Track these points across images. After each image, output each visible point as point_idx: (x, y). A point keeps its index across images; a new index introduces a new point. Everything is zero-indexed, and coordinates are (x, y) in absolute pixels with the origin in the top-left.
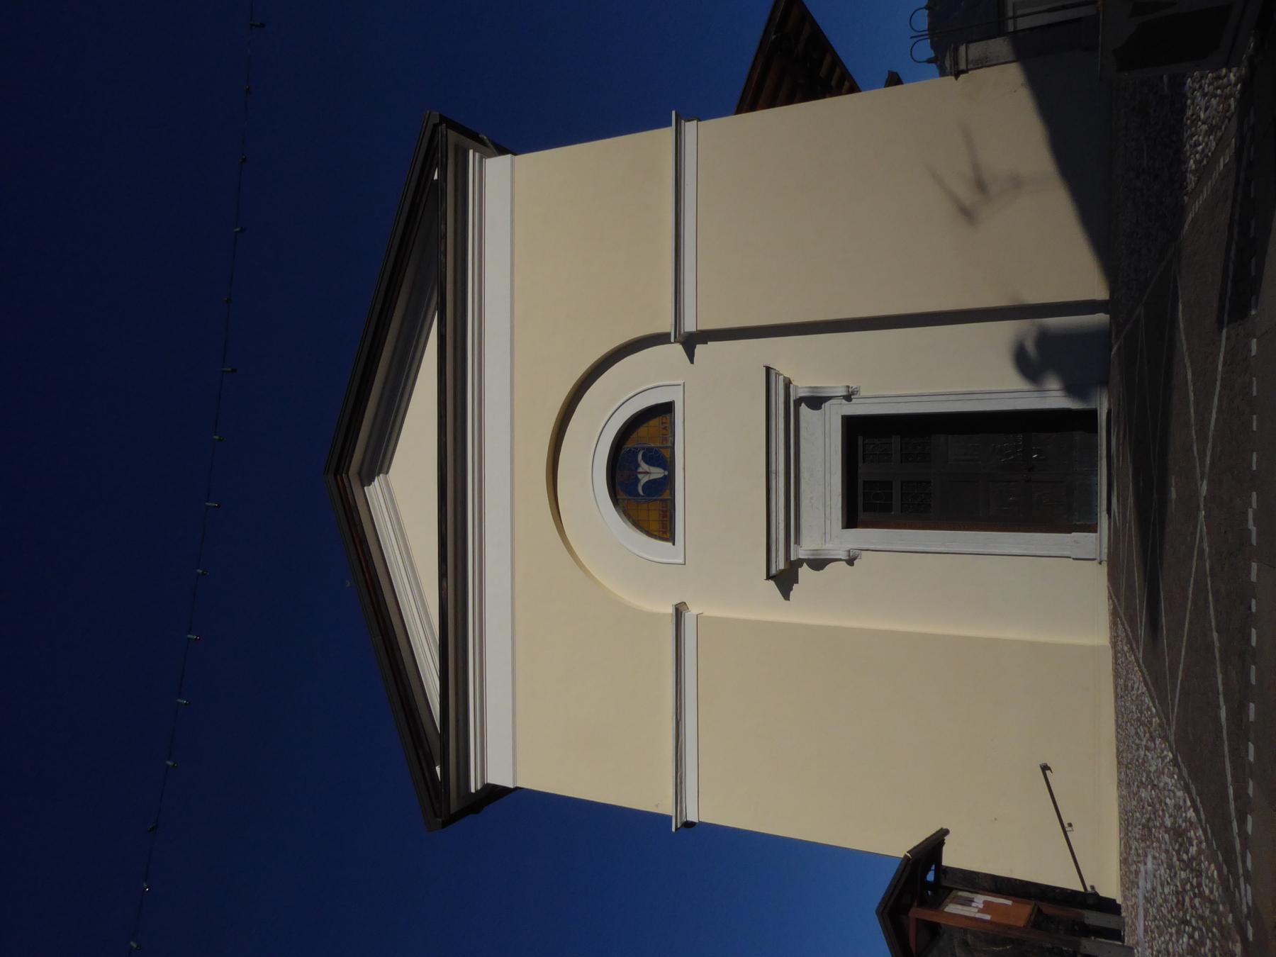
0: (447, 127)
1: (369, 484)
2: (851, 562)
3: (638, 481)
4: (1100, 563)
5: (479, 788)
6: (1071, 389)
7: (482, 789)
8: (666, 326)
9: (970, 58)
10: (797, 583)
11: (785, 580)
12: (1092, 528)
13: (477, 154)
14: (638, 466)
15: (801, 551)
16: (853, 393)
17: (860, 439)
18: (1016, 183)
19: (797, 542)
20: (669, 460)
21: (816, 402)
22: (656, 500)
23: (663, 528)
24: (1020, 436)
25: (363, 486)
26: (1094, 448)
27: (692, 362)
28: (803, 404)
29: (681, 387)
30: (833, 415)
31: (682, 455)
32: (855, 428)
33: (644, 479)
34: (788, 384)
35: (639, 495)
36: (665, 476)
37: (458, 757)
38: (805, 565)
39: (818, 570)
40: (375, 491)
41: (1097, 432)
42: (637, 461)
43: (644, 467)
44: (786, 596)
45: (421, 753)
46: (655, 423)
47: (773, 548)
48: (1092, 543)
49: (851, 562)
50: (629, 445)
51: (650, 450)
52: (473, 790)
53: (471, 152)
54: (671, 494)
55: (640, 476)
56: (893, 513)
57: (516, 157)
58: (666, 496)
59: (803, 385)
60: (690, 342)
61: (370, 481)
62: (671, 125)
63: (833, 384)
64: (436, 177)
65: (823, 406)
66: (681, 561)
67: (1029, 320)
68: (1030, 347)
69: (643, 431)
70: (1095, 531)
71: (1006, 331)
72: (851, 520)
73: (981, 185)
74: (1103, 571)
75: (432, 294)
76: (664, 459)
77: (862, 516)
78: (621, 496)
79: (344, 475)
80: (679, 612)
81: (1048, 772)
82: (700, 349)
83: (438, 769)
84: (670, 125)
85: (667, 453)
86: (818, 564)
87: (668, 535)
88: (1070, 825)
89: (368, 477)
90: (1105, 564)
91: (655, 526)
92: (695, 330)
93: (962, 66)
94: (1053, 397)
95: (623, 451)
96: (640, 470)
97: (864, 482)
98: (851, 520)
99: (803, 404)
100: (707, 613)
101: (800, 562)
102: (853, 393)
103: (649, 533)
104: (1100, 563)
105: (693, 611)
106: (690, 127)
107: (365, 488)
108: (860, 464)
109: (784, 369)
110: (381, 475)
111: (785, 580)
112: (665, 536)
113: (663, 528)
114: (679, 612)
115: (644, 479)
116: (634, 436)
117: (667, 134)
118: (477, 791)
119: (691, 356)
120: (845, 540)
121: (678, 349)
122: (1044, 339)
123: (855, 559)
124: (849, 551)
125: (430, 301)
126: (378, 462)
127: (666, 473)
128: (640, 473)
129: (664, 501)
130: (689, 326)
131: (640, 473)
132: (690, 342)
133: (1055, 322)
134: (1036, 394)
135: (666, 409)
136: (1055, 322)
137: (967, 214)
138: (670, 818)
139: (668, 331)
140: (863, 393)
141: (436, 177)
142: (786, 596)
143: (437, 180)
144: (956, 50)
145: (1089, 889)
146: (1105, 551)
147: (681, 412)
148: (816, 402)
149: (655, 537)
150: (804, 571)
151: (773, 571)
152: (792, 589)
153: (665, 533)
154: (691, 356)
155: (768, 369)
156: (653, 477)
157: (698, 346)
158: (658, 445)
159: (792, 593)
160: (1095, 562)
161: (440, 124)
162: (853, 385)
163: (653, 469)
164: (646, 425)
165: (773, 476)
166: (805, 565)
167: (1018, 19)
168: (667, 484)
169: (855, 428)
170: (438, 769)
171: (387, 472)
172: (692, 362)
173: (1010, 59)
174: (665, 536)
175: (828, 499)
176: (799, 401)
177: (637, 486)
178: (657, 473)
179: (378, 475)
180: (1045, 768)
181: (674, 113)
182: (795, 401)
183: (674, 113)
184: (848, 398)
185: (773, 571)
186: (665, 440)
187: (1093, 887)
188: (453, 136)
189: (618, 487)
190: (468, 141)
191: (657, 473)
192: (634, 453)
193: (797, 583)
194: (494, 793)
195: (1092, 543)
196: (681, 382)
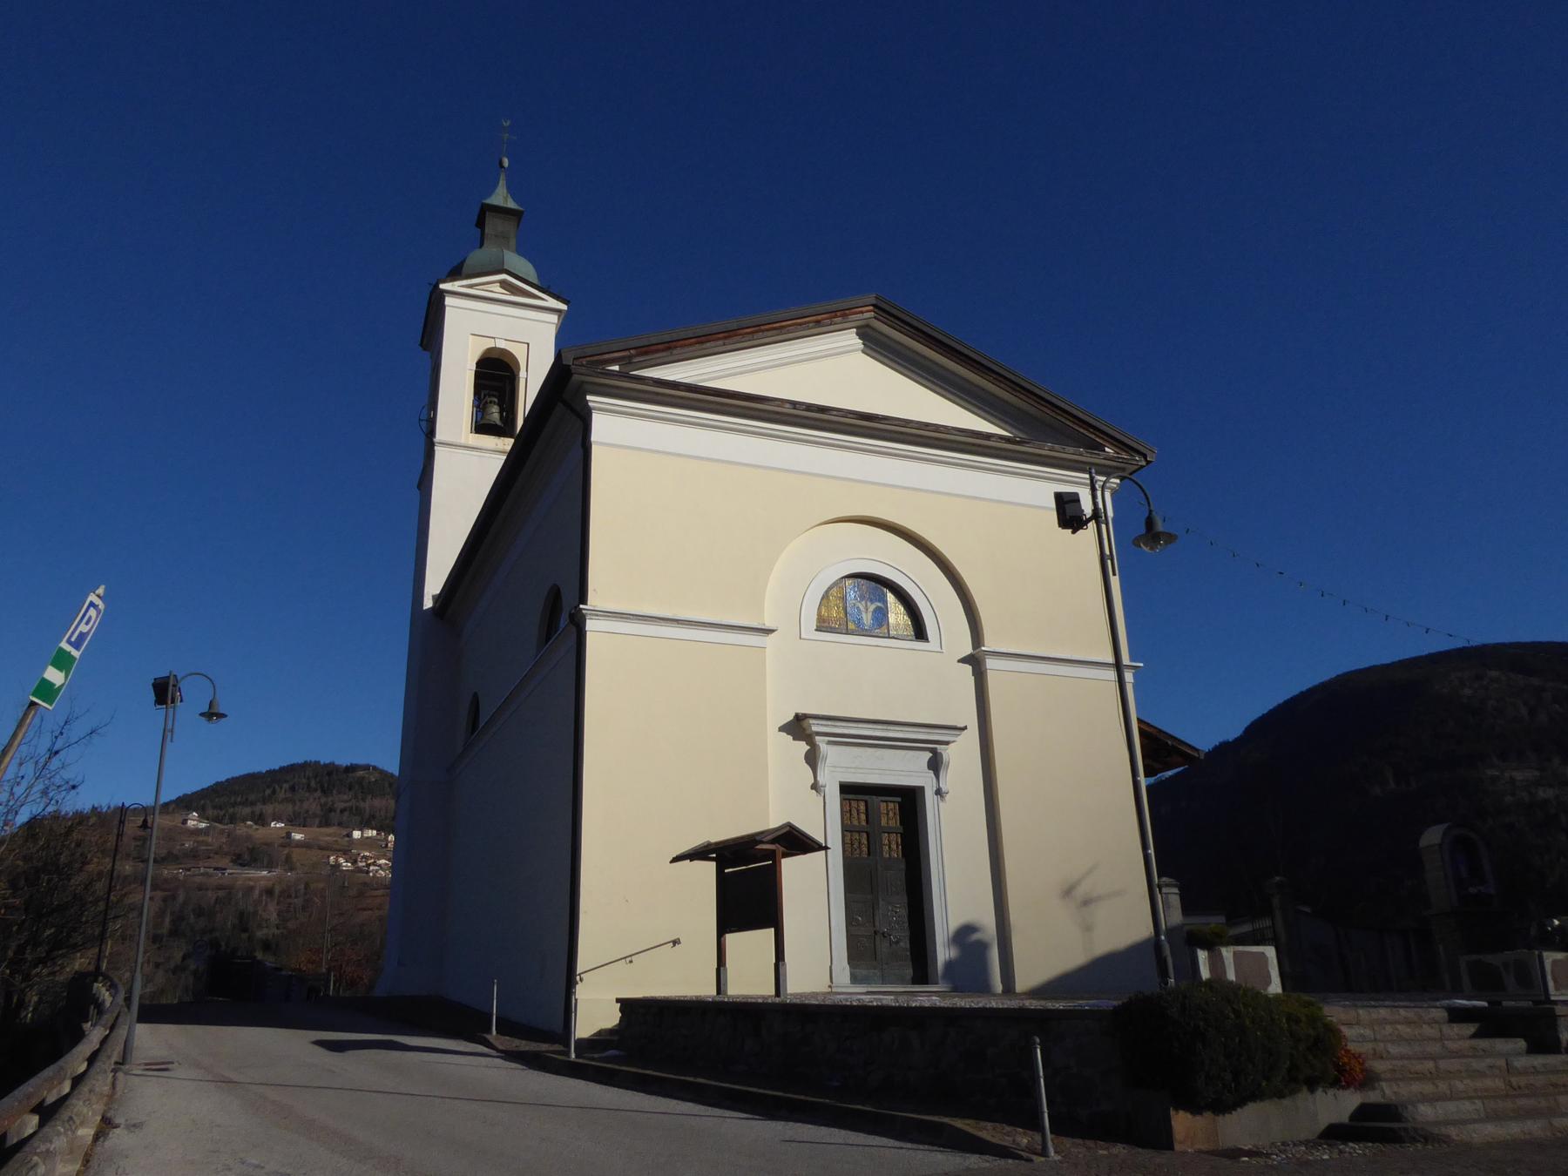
1: (857, 334)
2: (815, 787)
4: (830, 987)
6: (949, 965)
10: (794, 739)
11: (798, 727)
12: (855, 979)
16: (942, 797)
18: (1088, 928)
19: (829, 743)
21: (935, 764)
25: (857, 328)
28: (931, 755)
29: (939, 650)
31: (837, 640)
32: (909, 801)
34: (947, 743)
37: (617, 387)
39: (806, 762)
40: (850, 339)
44: (783, 729)
47: (829, 723)
49: (815, 787)
52: (588, 398)
57: (1220, 1118)
59: (949, 753)
61: (861, 335)
63: (949, 780)
65: (931, 771)
66: (803, 636)
67: (995, 933)
68: (975, 937)
71: (988, 920)
72: (847, 789)
73: (1086, 902)
75: (1010, 432)
80: (769, 631)
83: (616, 368)
86: (812, 759)
88: (631, 962)
89: (865, 334)
92: (988, 667)
93: (1164, 890)
94: (943, 952)
99: (931, 755)
102: (942, 797)
107: (855, 330)
110: (862, 346)
111: (798, 727)
114: (769, 631)
119: (963, 660)
121: (968, 650)
122: (983, 947)
125: (1006, 430)
126: (875, 345)
128: (866, 603)
130: (990, 663)
133: (994, 955)
134: (946, 940)
136: (994, 955)
137: (1068, 892)
138: (586, 604)
144: (1175, 886)
147: (920, 648)
148: (935, 764)
150: (803, 747)
152: (788, 734)
154: (963, 660)
159: (785, 734)
160: (830, 983)
162: (948, 797)
163: (870, 615)
165: (885, 727)
169: (909, 801)
170: (616, 368)
171: (863, 352)
175: (861, 771)
179: (863, 344)
180: (675, 942)
181: (1142, 665)
182: (936, 748)
183: (1142, 665)
184: (939, 792)
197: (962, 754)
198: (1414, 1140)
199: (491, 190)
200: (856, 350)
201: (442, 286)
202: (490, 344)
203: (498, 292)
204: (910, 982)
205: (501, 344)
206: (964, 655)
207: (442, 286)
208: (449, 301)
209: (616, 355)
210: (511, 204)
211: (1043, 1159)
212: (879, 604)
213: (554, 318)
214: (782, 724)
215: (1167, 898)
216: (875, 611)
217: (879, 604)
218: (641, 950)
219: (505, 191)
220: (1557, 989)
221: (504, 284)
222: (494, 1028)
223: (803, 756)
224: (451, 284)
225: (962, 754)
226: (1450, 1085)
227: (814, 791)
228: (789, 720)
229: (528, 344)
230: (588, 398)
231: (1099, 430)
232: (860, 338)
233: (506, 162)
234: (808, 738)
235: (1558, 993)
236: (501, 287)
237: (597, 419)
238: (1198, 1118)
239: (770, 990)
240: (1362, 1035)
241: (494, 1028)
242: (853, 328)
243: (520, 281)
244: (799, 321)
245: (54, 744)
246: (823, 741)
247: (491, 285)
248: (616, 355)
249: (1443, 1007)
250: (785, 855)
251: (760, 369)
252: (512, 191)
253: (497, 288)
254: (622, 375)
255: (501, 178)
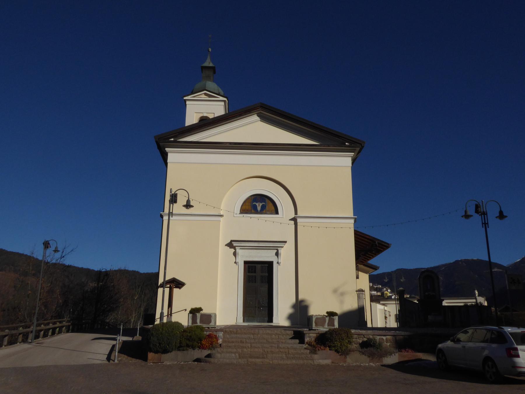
0: (360, 148)
1: (257, 116)
2: (235, 263)
3: (257, 202)
4: (236, 323)
5: (167, 151)
7: (166, 152)
8: (300, 214)
9: (360, 295)
10: (230, 248)
11: (230, 245)
12: (244, 321)
13: (353, 155)
14: (261, 203)
15: (238, 250)
17: (267, 265)
19: (240, 249)
20: (262, 212)
21: (277, 254)
22: (251, 208)
23: (244, 210)
24: (267, 305)
26: (264, 322)
27: (289, 220)
28: (277, 251)
29: (282, 217)
30: (273, 259)
32: (269, 266)
33: (257, 204)
34: (282, 247)
35: (253, 203)
36: (258, 211)
38: (234, 250)
41: (268, 322)
42: (263, 202)
43: (261, 204)
44: (226, 245)
45: (177, 134)
46: (273, 208)
48: (240, 321)
49: (235, 263)
50: (267, 200)
51: (265, 207)
52: (166, 149)
53: (353, 154)
54: (253, 212)
55: (258, 203)
56: (248, 273)
58: (253, 211)
59: (282, 251)
60: (294, 220)
62: (354, 216)
63: (282, 259)
64: (346, 144)
66: (235, 216)
69: (271, 204)
70: (243, 322)
72: (246, 263)
74: (235, 324)
76: (263, 211)
77: (247, 265)
78: (253, 197)
79: (260, 109)
80: (222, 216)
81: (185, 311)
82: (293, 222)
83: (172, 139)
84: (354, 216)
85: (264, 211)
86: (235, 254)
87: (242, 211)
90: (236, 324)
91: (244, 207)
95: (265, 198)
96: (260, 203)
97: (255, 266)
98: (246, 263)
99: (277, 251)
100: (221, 223)
101: (235, 249)
103: (242, 206)
104: (236, 323)
105: (221, 219)
106: (352, 221)
107: (256, 115)
108: (260, 265)
109: (286, 246)
111: (230, 245)
112: (241, 210)
113: (244, 210)
114: (222, 216)
115: (257, 204)
116: (270, 202)
117: (352, 215)
118: (166, 150)
119: (291, 220)
120: (241, 261)
121: (293, 215)
123: (236, 264)
124: (238, 262)
126: (264, 119)
127: (259, 211)
128: (259, 203)
129: (251, 211)
130: (299, 220)
131: (259, 203)
132: (294, 220)
135: (277, 212)
137: (335, 291)
139: (298, 214)
140: (279, 266)
141: (346, 144)
142: (226, 245)
143: (345, 144)
145: (157, 320)
146: (239, 324)
148: (277, 254)
149: (241, 208)
151: (233, 243)
152: (228, 247)
153: (242, 211)
155: (285, 242)
156: (258, 207)
157: (294, 222)
158: (267, 209)
161: (362, 146)
162: (281, 264)
163: (260, 207)
164: (273, 205)
166: (234, 250)
167: (395, 305)
168: (256, 212)
169: (269, 266)
170: (172, 139)
171: (260, 121)
172: (289, 220)
173: (359, 305)
174: (241, 210)
176: (278, 250)
177: (255, 202)
178: (259, 208)
181: (356, 217)
183: (356, 217)
184: (278, 263)
185: (233, 243)
186: (268, 211)
187: (157, 321)
188: (358, 149)
189: (255, 197)
190: (356, 154)
191: (259, 208)
192: (265, 202)
193: (230, 248)
194: (165, 156)
195: (240, 321)
196: (284, 217)
197: (287, 252)
198: (203, 362)
199: (204, 61)
200: (258, 121)
201: (185, 98)
202: (201, 115)
203: (204, 97)
204: (267, 321)
205: (205, 115)
206: (291, 218)
207: (185, 98)
208: (187, 103)
209: (172, 136)
210: (211, 65)
211: (113, 362)
212: (263, 203)
213: (223, 103)
214: (226, 243)
215: (359, 295)
216: (262, 205)
217: (263, 203)
218: (180, 312)
219: (210, 60)
220: (316, 326)
221: (205, 94)
222: (138, 334)
223: (233, 253)
224: (187, 97)
225: (287, 252)
226: (242, 350)
227: (235, 264)
228: (229, 242)
229: (214, 113)
230: (166, 149)
231: (344, 138)
232: (258, 117)
233: (210, 50)
234: (234, 248)
235: (316, 327)
236: (205, 95)
237: (169, 155)
238: (156, 354)
239: (371, 327)
240: (249, 337)
241: (138, 334)
242: (255, 114)
243: (212, 93)
244: (234, 115)
245: (62, 255)
246: (238, 248)
247: (201, 95)
248: (172, 136)
249: (293, 330)
250: (174, 288)
251: (235, 129)
252: (212, 61)
253: (204, 96)
254: (174, 142)
255: (208, 58)
